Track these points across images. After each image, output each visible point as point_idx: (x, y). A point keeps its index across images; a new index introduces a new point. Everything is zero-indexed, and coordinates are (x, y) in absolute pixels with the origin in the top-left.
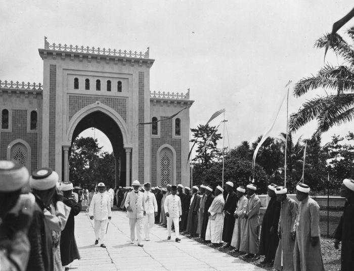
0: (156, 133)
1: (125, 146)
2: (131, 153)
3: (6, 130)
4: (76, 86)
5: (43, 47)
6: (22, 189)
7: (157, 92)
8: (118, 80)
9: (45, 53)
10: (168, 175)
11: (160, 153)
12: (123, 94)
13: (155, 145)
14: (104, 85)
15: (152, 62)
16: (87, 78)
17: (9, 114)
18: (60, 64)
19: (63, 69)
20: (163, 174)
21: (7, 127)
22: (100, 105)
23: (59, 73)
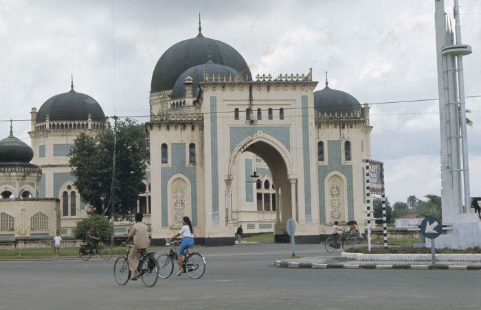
0: (321, 159)
1: (290, 177)
2: (296, 184)
4: (237, 117)
6: (266, 92)
10: (339, 204)
12: (285, 122)
13: (323, 173)
19: (224, 100)
21: (166, 162)
22: (261, 135)
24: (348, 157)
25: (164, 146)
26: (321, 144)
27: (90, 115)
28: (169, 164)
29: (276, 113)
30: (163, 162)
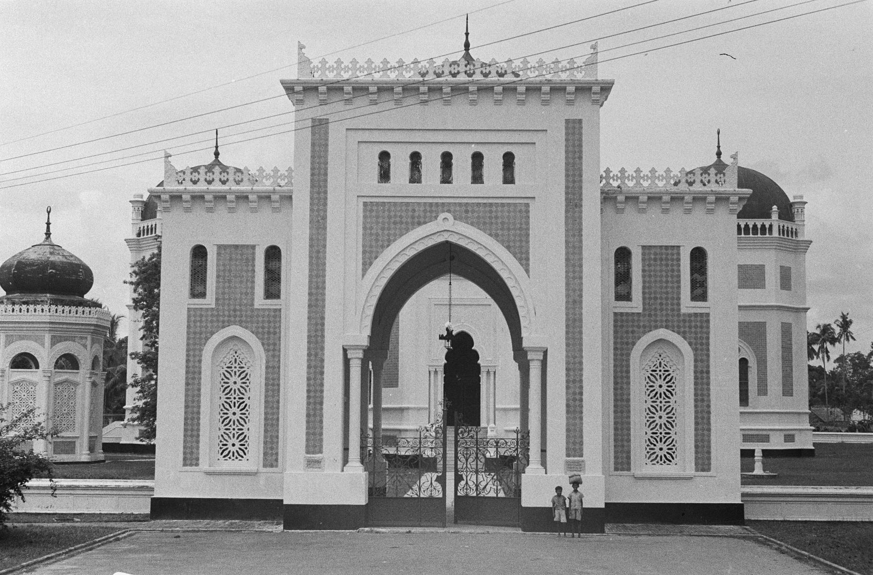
0: (624, 296)
3: (275, 301)
4: (385, 175)
5: (292, 75)
7: (630, 172)
8: (378, 149)
9: (298, 88)
11: (213, 356)
13: (624, 332)
14: (431, 166)
15: (606, 88)
16: (416, 148)
17: (209, 257)
18: (341, 117)
20: (651, 423)
21: (203, 295)
22: (448, 226)
23: (336, 135)
24: (699, 290)
25: (199, 253)
26: (623, 255)
27: (775, 208)
28: (210, 301)
29: (493, 167)
30: (619, 297)
